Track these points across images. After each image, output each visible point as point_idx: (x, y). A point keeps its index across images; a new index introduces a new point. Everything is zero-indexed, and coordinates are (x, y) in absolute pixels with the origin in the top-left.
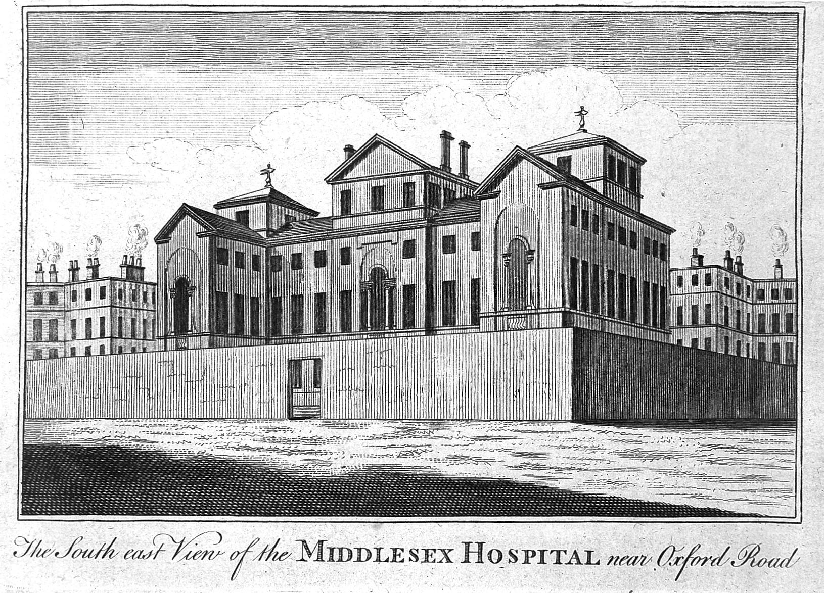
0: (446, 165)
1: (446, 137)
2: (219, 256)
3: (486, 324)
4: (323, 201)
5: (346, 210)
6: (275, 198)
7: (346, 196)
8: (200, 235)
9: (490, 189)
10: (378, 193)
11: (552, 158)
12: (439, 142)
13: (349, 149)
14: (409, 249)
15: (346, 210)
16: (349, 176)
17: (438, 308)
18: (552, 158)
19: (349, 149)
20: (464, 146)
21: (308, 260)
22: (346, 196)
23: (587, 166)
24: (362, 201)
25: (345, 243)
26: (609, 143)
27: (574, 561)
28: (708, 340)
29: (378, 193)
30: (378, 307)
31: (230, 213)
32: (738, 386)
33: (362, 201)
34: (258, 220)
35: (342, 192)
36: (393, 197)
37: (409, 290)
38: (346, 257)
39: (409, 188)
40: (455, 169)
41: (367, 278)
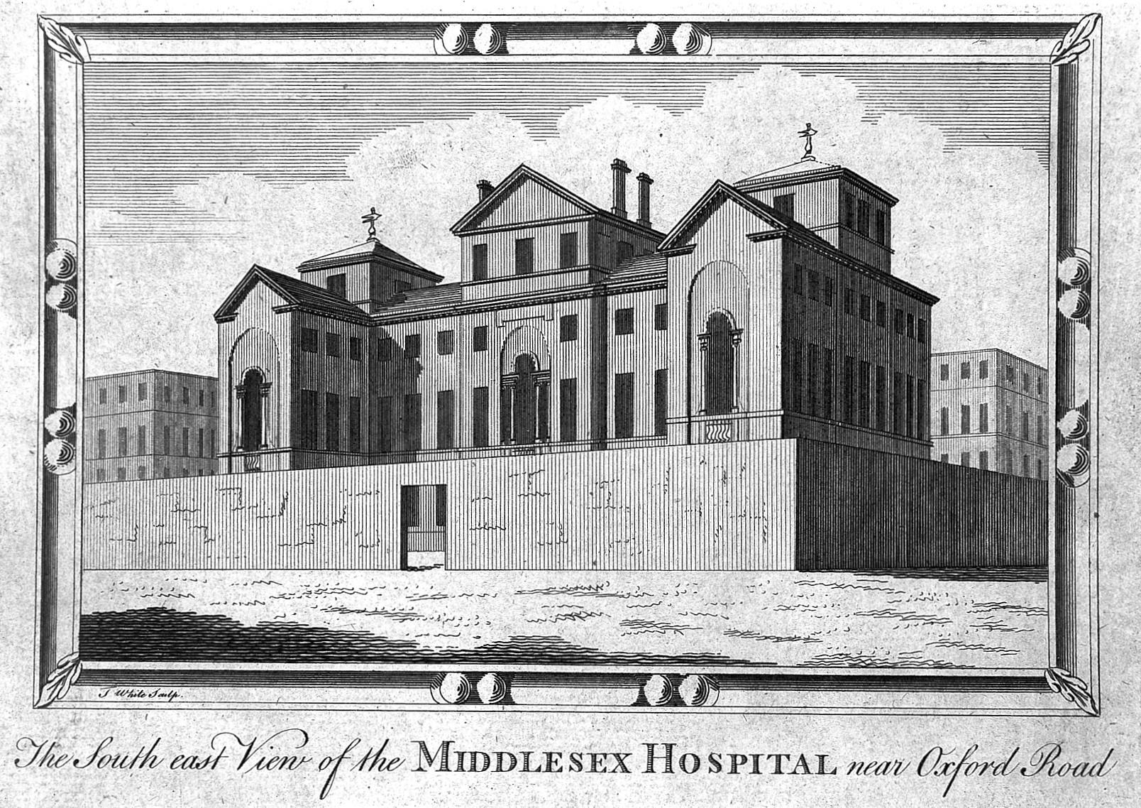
1: (620, 168)
2: (304, 341)
3: (676, 432)
4: (446, 259)
5: (480, 275)
7: (480, 253)
9: (681, 242)
10: (524, 250)
11: (767, 198)
13: (485, 187)
14: (569, 329)
17: (614, 422)
18: (767, 198)
19: (485, 187)
21: (429, 347)
22: (480, 253)
23: (817, 211)
24: (501, 259)
27: (801, 770)
28: (983, 456)
29: (524, 250)
30: (525, 412)
31: (318, 280)
32: (987, 522)
36: (547, 253)
37: (569, 387)
39: (568, 243)
41: (510, 369)
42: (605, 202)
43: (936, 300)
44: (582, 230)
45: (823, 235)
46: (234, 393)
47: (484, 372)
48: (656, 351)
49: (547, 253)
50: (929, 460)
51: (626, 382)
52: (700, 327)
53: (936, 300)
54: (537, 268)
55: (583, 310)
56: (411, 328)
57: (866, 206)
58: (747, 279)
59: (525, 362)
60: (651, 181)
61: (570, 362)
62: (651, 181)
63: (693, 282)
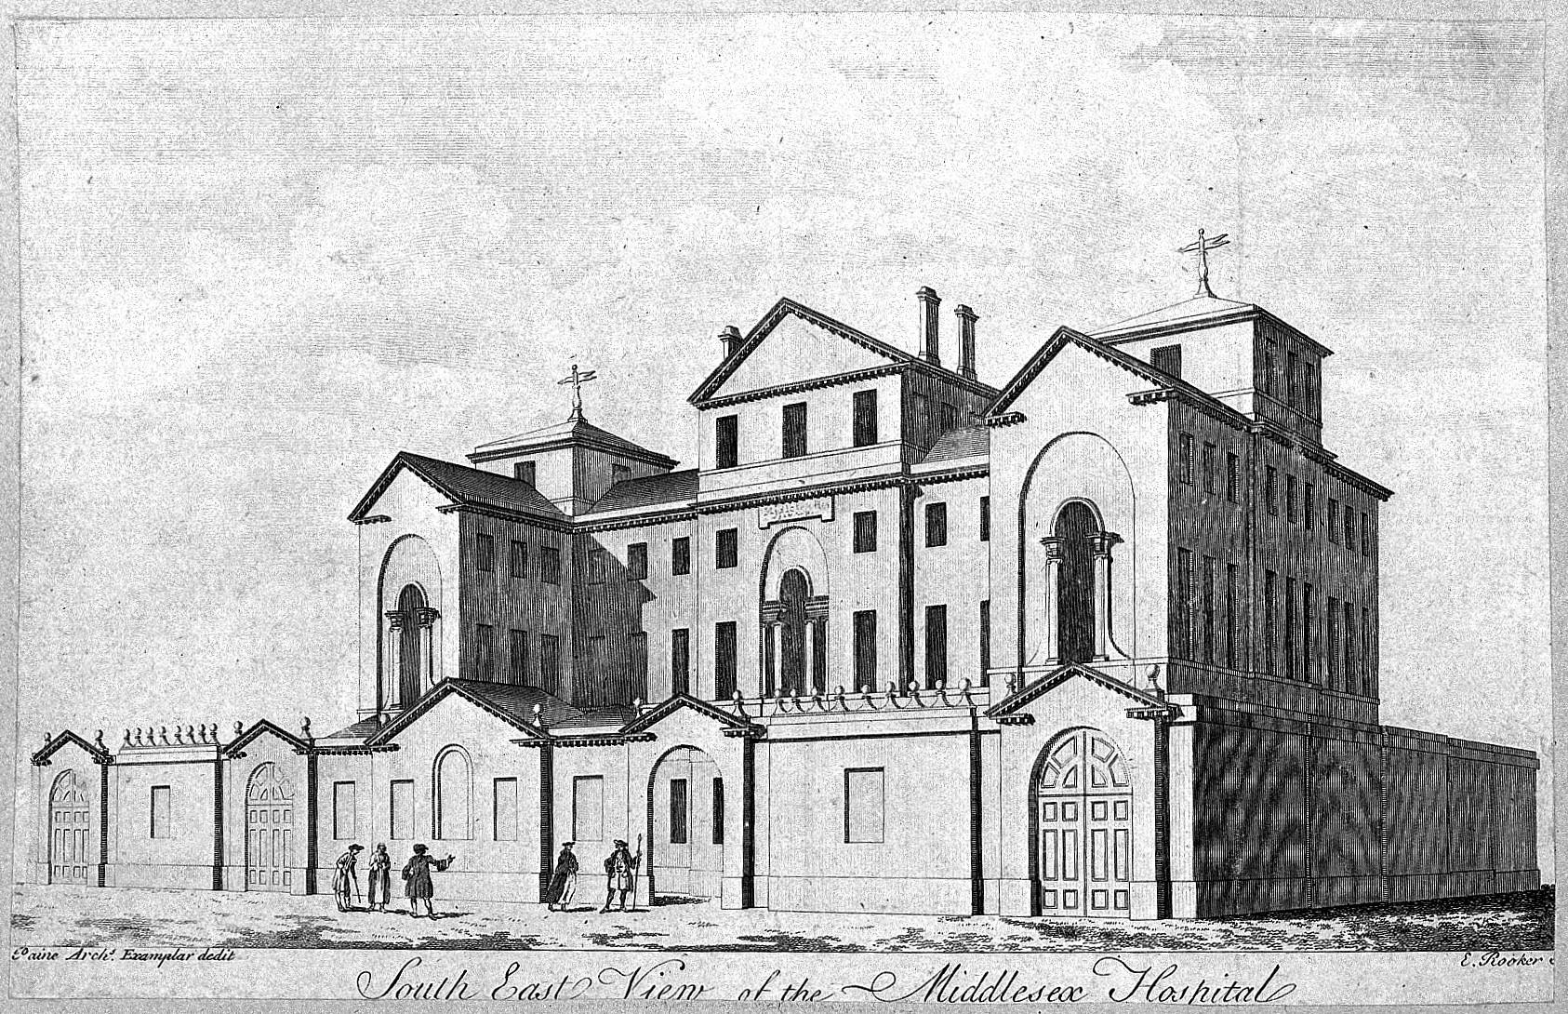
0: (933, 354)
1: (931, 299)
2: (477, 552)
4: (689, 443)
5: (728, 454)
6: (585, 438)
7: (728, 429)
8: (445, 510)
10: (795, 424)
11: (1142, 351)
12: (918, 309)
14: (865, 539)
15: (728, 454)
16: (724, 391)
18: (1142, 351)
20: (968, 316)
21: (661, 557)
22: (728, 429)
23: (1223, 366)
24: (761, 429)
25: (726, 521)
26: (1264, 322)
29: (795, 424)
31: (506, 468)
33: (761, 429)
34: (555, 478)
35: (721, 534)
36: (831, 417)
37: (865, 623)
38: (727, 549)
39: (866, 407)
40: (950, 358)
41: (773, 593)
42: (912, 342)
43: (1386, 494)
44: (889, 393)
45: (1231, 402)
46: (387, 624)
47: (737, 596)
48: (983, 575)
49: (831, 417)
50: (1374, 729)
51: (937, 615)
52: (391, 604)
53: (1386, 494)
54: (812, 446)
55: (886, 504)
56: (638, 535)
57: (1288, 356)
58: (1112, 450)
59: (796, 582)
60: (975, 319)
61: (855, 584)
62: (975, 319)
63: (1031, 471)
